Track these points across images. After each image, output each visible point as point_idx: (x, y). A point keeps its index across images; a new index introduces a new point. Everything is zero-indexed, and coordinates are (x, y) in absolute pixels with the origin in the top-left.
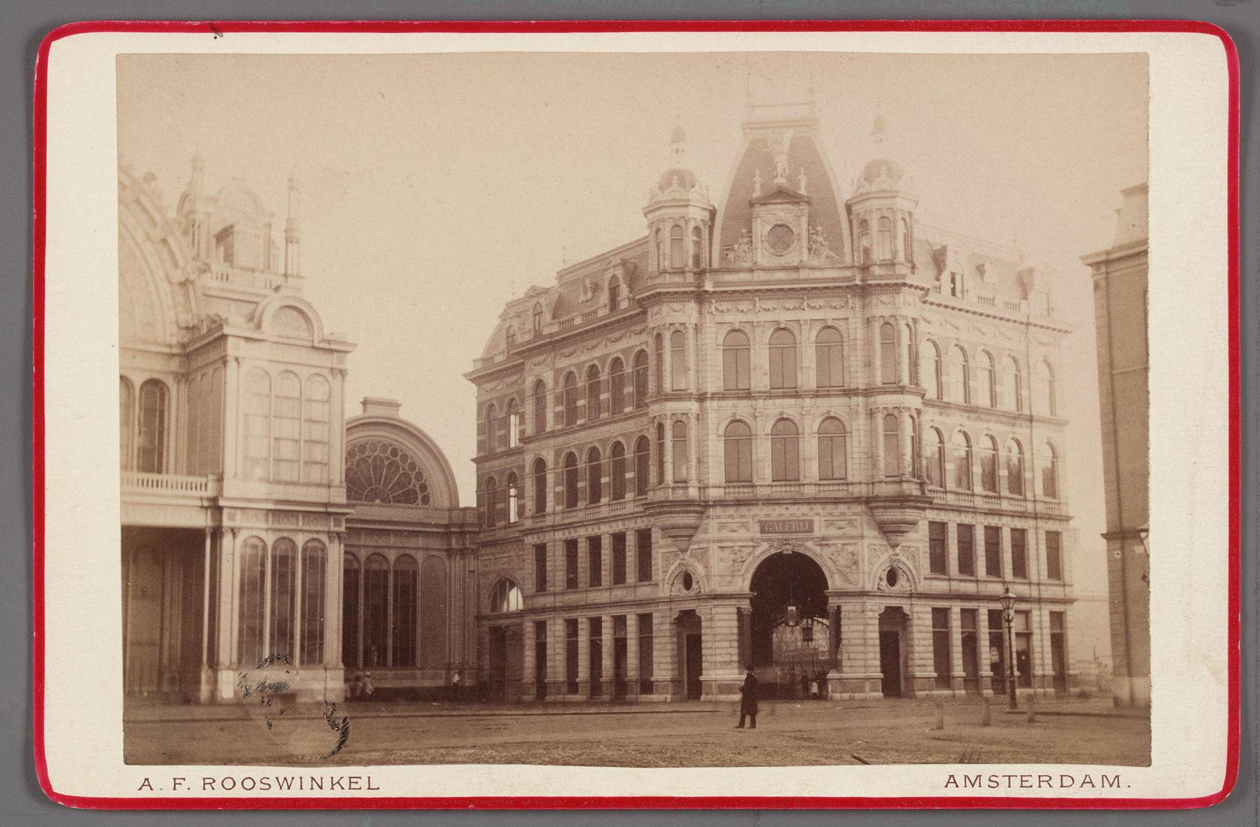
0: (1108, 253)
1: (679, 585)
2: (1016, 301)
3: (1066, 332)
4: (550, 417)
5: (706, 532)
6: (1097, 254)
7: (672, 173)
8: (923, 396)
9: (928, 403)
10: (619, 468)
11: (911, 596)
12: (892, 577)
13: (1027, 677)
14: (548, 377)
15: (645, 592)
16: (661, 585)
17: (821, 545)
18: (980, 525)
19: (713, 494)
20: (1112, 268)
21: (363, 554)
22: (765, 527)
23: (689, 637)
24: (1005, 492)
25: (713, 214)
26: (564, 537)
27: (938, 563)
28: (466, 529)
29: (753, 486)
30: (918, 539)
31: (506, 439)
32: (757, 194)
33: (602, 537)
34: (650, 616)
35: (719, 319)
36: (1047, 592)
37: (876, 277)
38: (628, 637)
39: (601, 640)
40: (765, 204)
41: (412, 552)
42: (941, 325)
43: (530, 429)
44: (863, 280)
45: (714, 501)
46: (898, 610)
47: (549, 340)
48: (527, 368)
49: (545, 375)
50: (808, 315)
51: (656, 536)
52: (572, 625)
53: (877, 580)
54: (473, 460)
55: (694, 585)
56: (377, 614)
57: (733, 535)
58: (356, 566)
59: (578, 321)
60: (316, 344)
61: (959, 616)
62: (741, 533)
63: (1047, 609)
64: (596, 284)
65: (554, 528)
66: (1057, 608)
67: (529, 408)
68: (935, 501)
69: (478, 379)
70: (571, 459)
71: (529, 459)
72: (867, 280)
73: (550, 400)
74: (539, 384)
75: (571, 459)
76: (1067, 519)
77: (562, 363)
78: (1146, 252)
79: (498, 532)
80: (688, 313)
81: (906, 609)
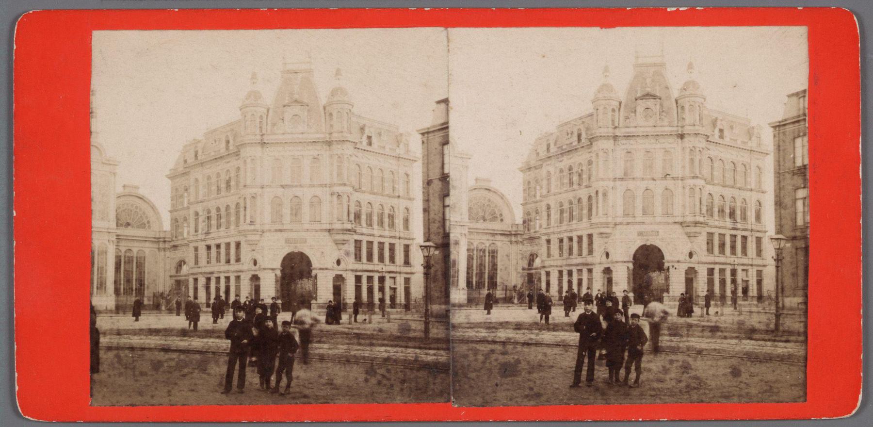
0: (428, 129)
1: (604, 257)
2: (746, 141)
3: (415, 161)
4: (201, 193)
5: (615, 235)
6: (424, 129)
7: (603, 85)
8: (705, 180)
9: (708, 183)
10: (219, 217)
11: (699, 263)
12: (691, 255)
13: (393, 304)
14: (200, 178)
18: (728, 233)
19: (267, 227)
20: (430, 135)
21: (123, 249)
22: (288, 241)
23: (608, 278)
24: (739, 220)
25: (620, 103)
27: (710, 250)
29: (282, 224)
30: (702, 239)
31: (182, 203)
32: (639, 95)
36: (755, 262)
40: (642, 99)
41: (143, 249)
43: (544, 192)
44: (330, 138)
46: (693, 268)
48: (543, 166)
50: (658, 146)
51: (243, 245)
55: (258, 265)
56: (128, 273)
58: (120, 254)
59: (213, 154)
60: (104, 161)
61: (718, 271)
63: (755, 269)
64: (572, 132)
65: (554, 233)
66: (760, 268)
67: (545, 183)
68: (357, 231)
69: (172, 177)
70: (561, 205)
71: (192, 212)
73: (201, 187)
74: (197, 180)
75: (561, 205)
76: (413, 239)
78: (447, 128)
80: (257, 151)
81: (344, 276)
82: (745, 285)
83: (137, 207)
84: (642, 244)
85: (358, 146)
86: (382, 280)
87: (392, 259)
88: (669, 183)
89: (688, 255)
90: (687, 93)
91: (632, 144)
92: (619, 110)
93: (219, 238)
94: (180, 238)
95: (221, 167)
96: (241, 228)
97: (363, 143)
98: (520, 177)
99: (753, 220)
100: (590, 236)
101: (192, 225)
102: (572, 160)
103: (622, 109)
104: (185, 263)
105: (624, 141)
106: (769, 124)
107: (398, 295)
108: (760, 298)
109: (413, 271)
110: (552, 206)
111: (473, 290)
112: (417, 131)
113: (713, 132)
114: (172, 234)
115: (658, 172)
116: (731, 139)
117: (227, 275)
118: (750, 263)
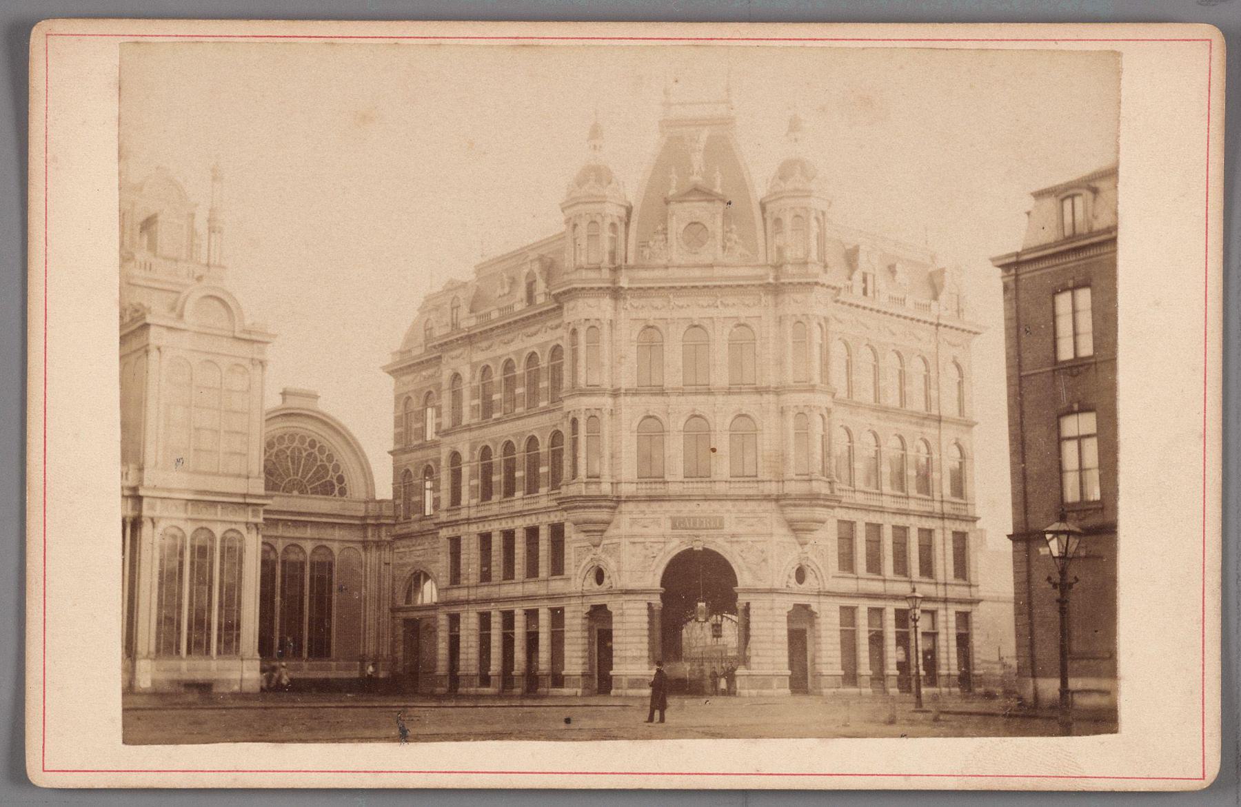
0: (1018, 254)
1: (591, 581)
3: (976, 333)
9: (838, 403)
11: (819, 594)
12: (800, 575)
14: (466, 373)
21: (280, 546)
25: (629, 211)
26: (478, 531)
27: (847, 562)
28: (382, 521)
30: (827, 539)
35: (634, 316)
39: (513, 634)
43: (446, 422)
44: (776, 278)
46: (806, 607)
52: (485, 619)
55: (606, 581)
58: (272, 556)
60: (237, 335)
63: (953, 609)
65: (468, 521)
67: (446, 400)
68: (844, 500)
74: (456, 377)
75: (486, 452)
76: (974, 520)
80: (603, 308)
81: (814, 607)
82: (929, 645)
83: (313, 444)
84: (684, 548)
85: (842, 298)
86: (903, 618)
87: (927, 568)
88: (747, 403)
89: (793, 574)
90: (789, 185)
91: (652, 310)
92: (627, 224)
93: (536, 512)
94: (415, 517)
95: (519, 345)
96: (566, 491)
97: (855, 290)
98: (387, 387)
99: (947, 490)
100: (557, 532)
101: (445, 485)
102: (512, 348)
103: (633, 225)
104: (427, 577)
105: (636, 302)
106: (993, 260)
107: (943, 661)
108: (966, 679)
109: (976, 596)
110: (465, 456)
111: (181, 658)
112: (993, 260)
113: (850, 279)
114: (396, 507)
115: (720, 377)
116: (890, 298)
117: (530, 605)
118: (941, 594)
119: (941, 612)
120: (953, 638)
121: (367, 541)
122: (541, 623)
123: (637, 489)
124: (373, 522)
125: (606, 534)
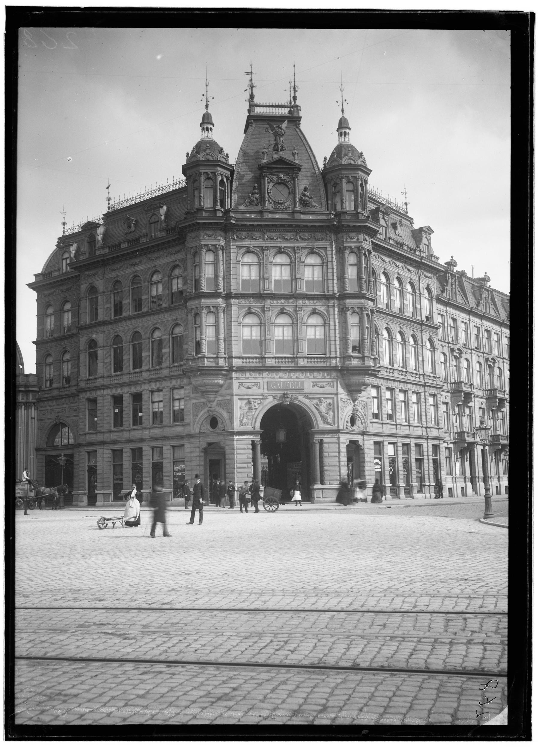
1: (207, 427)
12: (353, 421)
15: (137, 434)
16: (192, 425)
17: (309, 398)
26: (111, 394)
28: (31, 389)
33: (143, 393)
34: (140, 450)
35: (239, 244)
37: (347, 220)
38: (164, 461)
39: (142, 464)
42: (376, 258)
45: (237, 367)
47: (102, 258)
49: (97, 283)
52: (117, 454)
53: (346, 423)
54: (34, 342)
55: (219, 425)
57: (249, 391)
62: (255, 390)
72: (341, 222)
77: (111, 275)
79: (144, 374)
81: (361, 443)
104: (64, 425)
119: (425, 446)
120: (431, 461)
121: (29, 402)
122: (124, 458)
123: (243, 362)
124: (23, 389)
125: (220, 393)
